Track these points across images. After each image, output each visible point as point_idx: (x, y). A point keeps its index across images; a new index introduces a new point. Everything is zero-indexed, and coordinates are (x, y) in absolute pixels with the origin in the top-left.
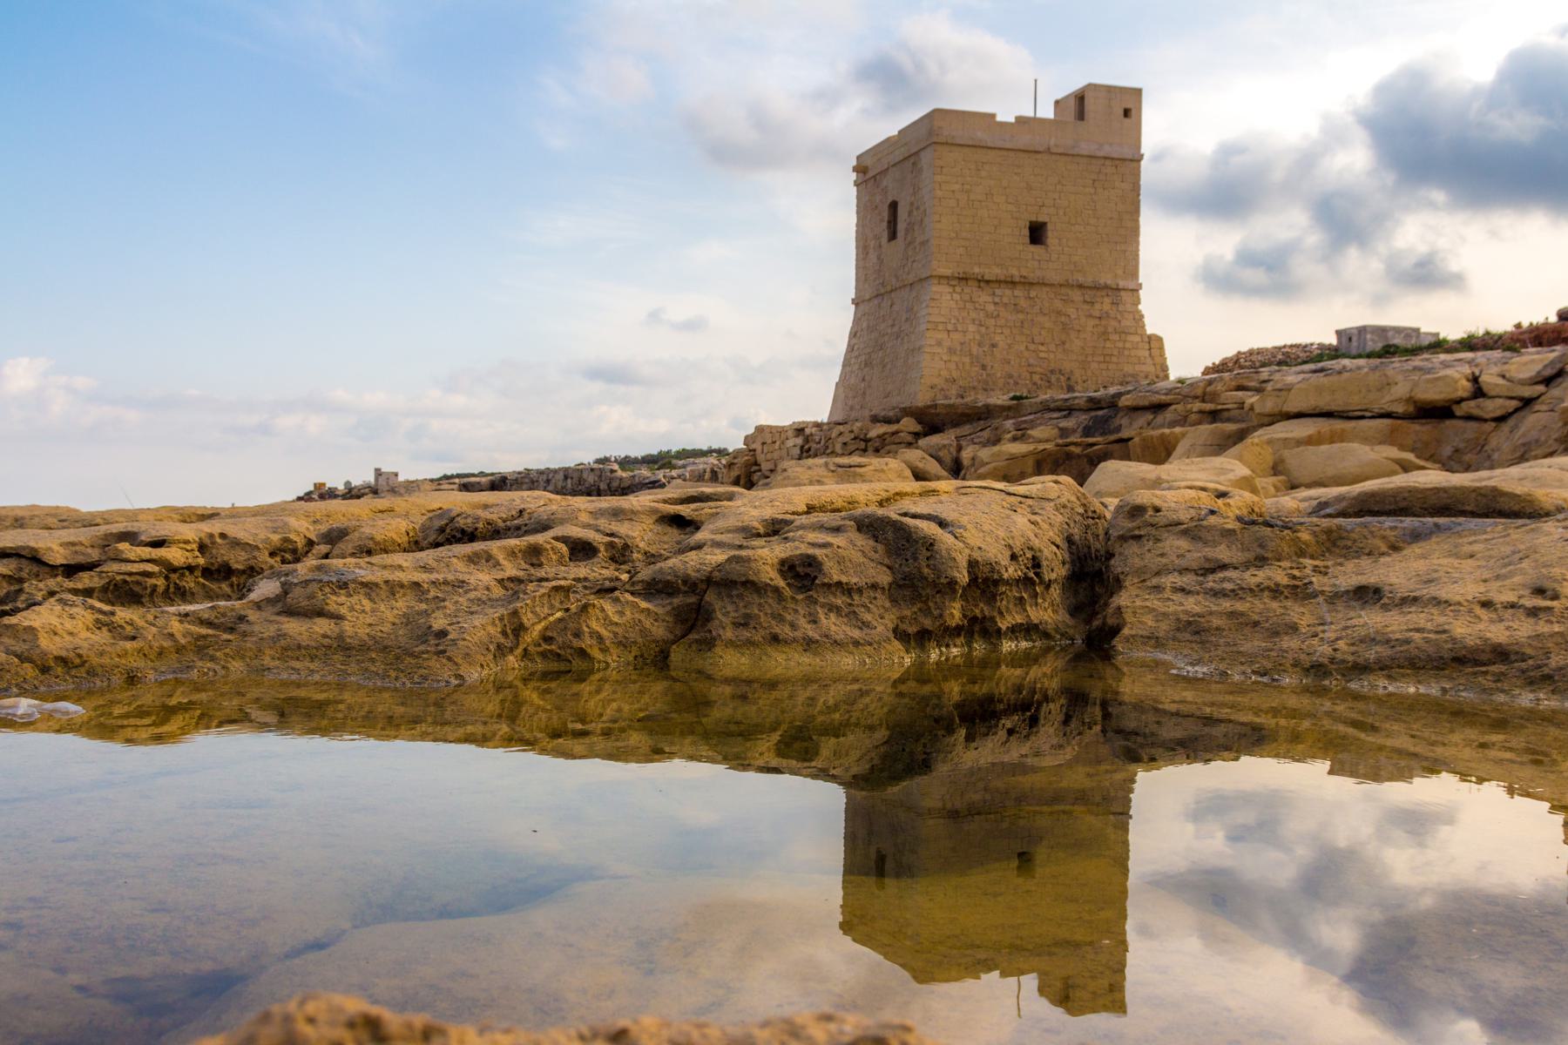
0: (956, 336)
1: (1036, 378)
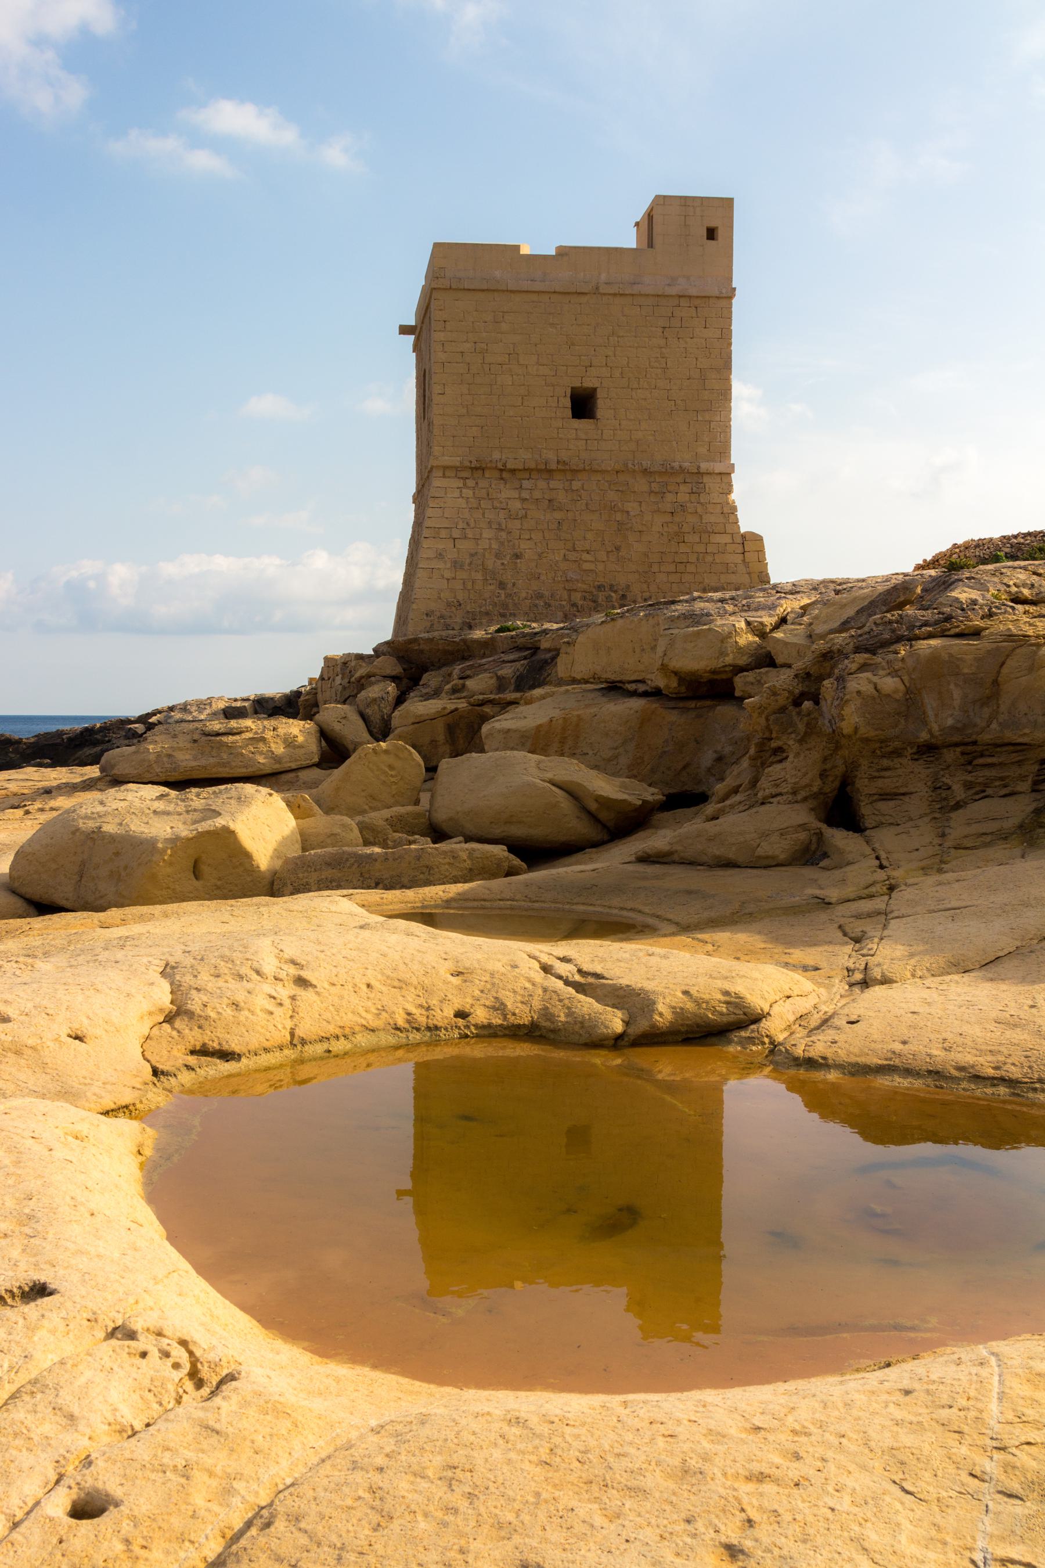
0: (464, 545)
1: (577, 597)
